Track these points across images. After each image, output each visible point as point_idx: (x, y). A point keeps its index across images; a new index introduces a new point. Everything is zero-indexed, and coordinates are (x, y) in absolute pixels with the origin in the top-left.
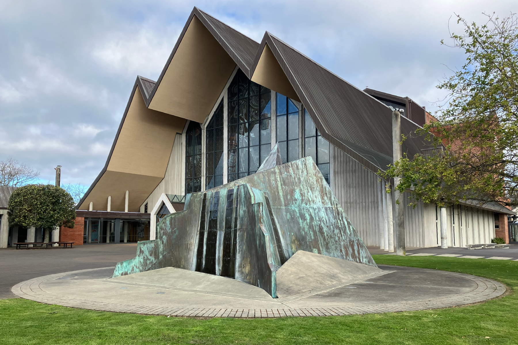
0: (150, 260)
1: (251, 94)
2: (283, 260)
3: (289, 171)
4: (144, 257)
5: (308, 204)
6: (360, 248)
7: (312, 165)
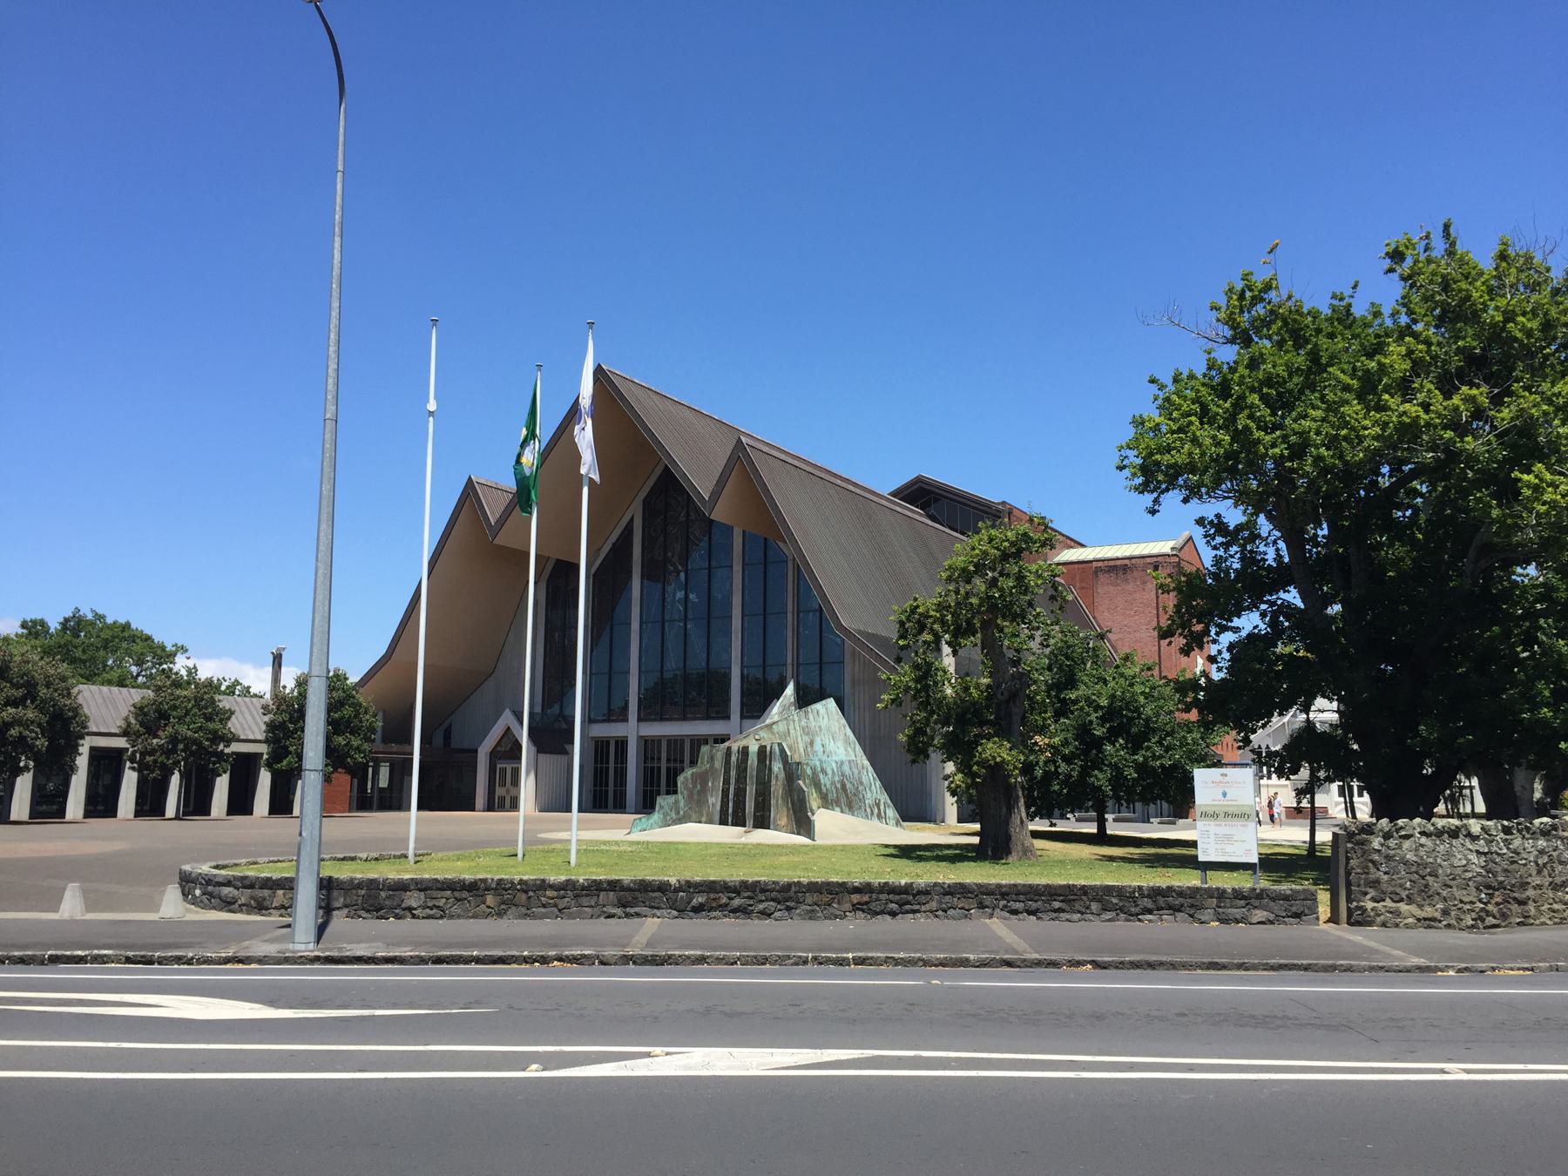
2: (813, 814)
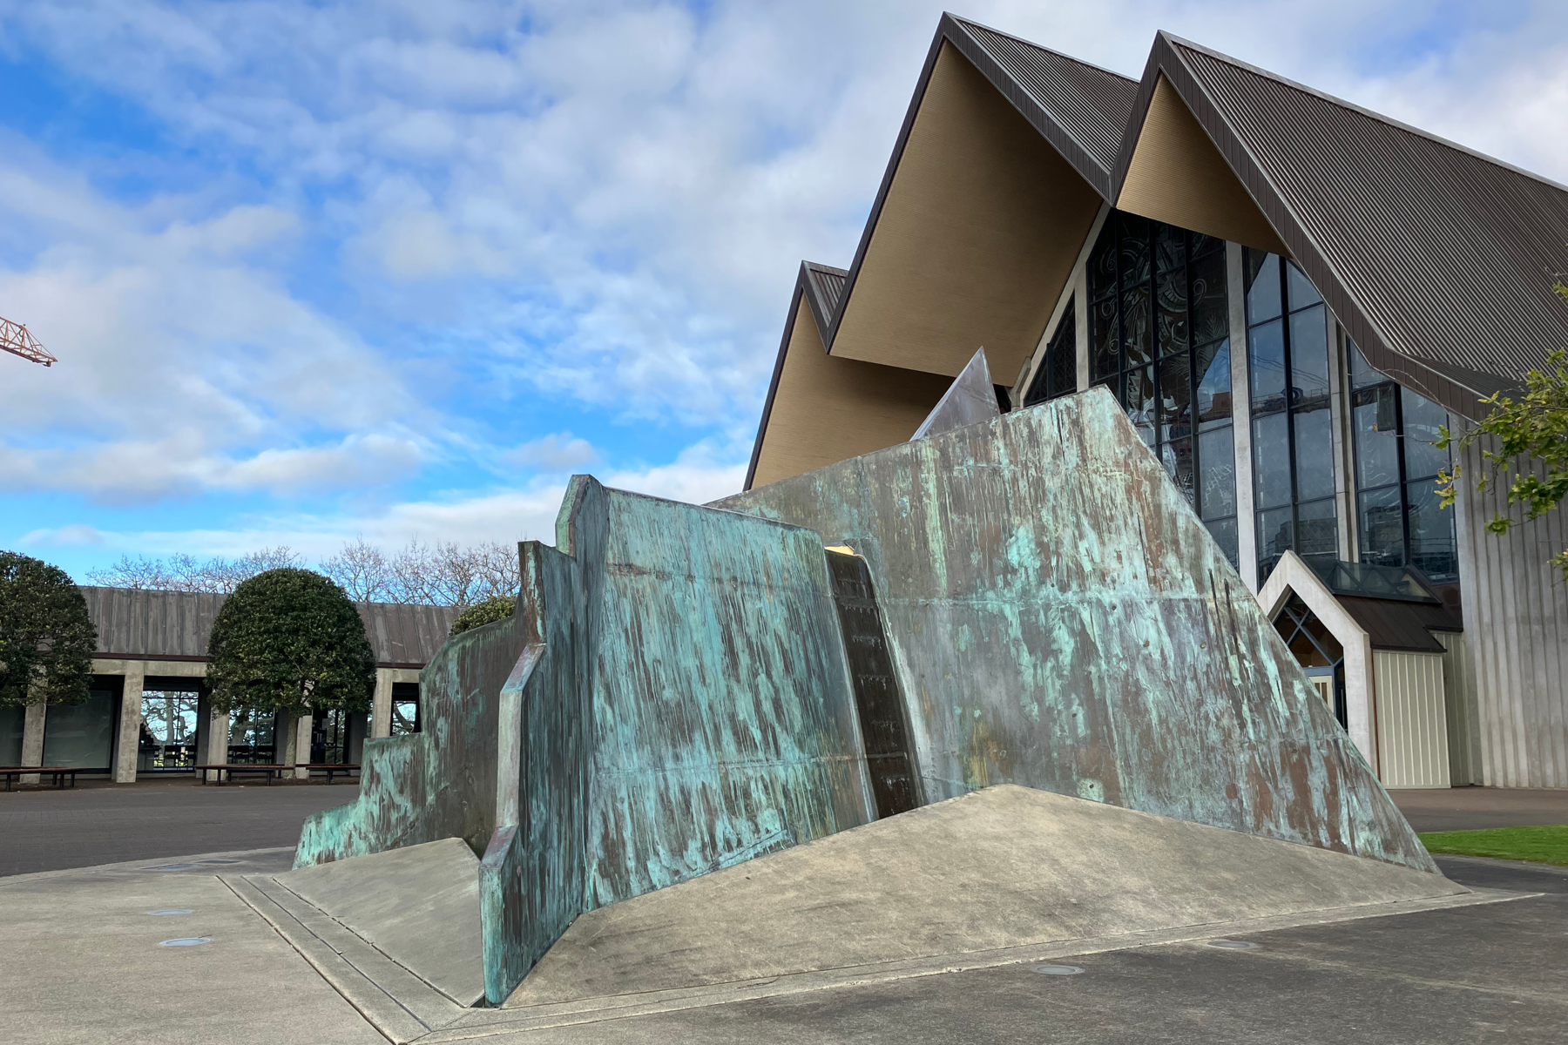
0: (398, 807)
1: (1162, 267)
3: (987, 453)
4: (382, 800)
5: (1074, 586)
6: (1340, 781)
7: (1110, 423)
